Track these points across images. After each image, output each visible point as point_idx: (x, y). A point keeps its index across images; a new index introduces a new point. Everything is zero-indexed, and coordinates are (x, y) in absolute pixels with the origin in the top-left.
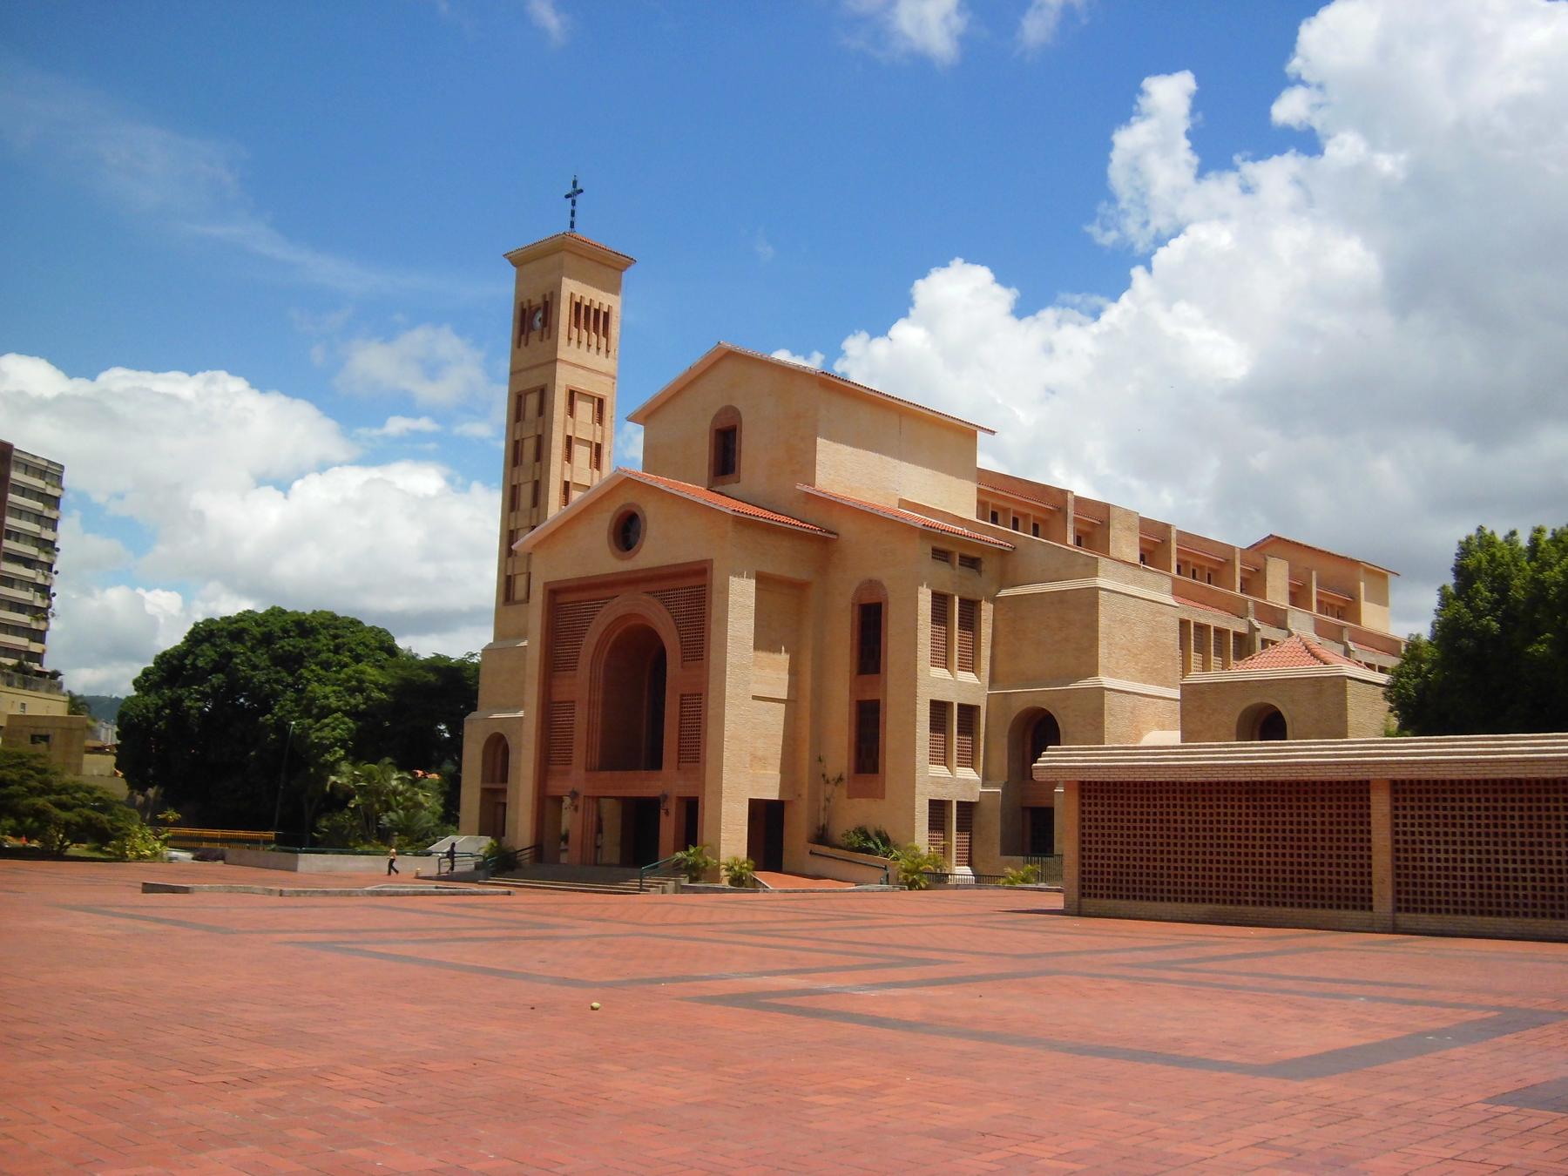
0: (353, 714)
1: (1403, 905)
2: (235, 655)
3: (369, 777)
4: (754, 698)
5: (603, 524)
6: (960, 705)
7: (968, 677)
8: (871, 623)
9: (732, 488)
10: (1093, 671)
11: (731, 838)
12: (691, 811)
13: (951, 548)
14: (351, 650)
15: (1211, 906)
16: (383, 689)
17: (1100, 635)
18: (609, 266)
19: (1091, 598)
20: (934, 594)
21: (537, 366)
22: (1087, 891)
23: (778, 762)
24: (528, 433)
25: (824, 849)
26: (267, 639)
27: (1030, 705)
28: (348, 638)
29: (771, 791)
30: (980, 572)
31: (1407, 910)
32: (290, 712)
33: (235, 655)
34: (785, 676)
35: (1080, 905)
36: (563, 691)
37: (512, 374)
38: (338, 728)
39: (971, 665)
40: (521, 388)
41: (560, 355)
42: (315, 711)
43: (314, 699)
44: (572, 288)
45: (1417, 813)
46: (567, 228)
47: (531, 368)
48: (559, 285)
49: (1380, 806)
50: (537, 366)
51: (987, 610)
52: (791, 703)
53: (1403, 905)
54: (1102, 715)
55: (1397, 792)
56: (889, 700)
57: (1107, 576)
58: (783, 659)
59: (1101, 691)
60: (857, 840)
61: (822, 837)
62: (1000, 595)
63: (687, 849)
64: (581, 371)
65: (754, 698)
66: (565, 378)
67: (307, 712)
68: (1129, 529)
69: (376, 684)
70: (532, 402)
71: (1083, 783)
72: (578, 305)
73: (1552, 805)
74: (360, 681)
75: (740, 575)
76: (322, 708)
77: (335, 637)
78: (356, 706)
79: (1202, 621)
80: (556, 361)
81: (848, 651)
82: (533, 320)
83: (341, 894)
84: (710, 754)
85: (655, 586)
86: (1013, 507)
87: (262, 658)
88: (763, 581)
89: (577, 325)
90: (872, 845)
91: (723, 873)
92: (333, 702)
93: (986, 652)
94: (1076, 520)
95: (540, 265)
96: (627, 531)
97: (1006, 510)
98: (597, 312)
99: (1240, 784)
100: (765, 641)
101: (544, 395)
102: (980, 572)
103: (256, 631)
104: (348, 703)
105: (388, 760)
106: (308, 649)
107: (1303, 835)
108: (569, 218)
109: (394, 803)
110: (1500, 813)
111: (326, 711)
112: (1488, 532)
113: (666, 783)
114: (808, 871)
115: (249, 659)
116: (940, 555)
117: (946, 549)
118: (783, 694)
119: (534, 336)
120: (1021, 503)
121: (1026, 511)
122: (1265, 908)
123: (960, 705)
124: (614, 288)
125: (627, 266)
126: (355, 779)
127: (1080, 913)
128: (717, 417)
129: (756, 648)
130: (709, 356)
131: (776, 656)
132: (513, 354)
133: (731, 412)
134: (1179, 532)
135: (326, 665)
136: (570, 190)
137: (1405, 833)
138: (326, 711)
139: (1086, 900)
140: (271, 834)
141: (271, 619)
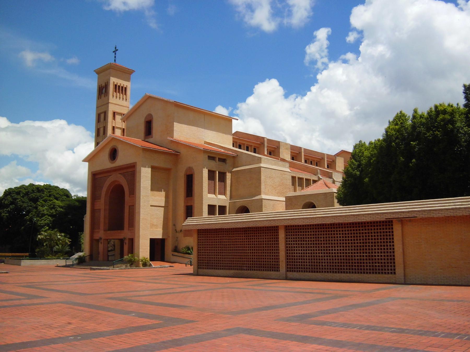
0: (52, 216)
1: (289, 269)
2: (18, 199)
3: (50, 235)
4: (151, 206)
5: (106, 155)
6: (219, 206)
7: (222, 197)
8: (190, 180)
9: (151, 140)
10: (260, 194)
11: (144, 251)
12: (132, 241)
13: (215, 156)
14: (54, 196)
15: (236, 271)
16: (62, 207)
17: (262, 182)
18: (126, 73)
19: (258, 171)
20: (209, 171)
21: (104, 105)
22: (200, 267)
23: (162, 226)
24: (101, 126)
25: (176, 254)
26: (27, 194)
27: (244, 205)
28: (54, 192)
29: (158, 235)
30: (226, 163)
31: (290, 271)
32: (34, 215)
33: (18, 199)
34: (164, 199)
35: (198, 271)
36: (97, 207)
37: (97, 108)
38: (47, 220)
39: (224, 194)
40: (99, 112)
41: (110, 101)
42: (40, 215)
43: (40, 211)
44: (113, 80)
45: (267, 237)
46: (113, 62)
47: (102, 106)
48: (109, 79)
49: (282, 235)
50: (104, 105)
51: (229, 176)
52: (166, 207)
53: (289, 269)
54: (262, 207)
55: (287, 230)
56: (195, 205)
57: (265, 163)
58: (163, 193)
59: (262, 199)
60: (185, 250)
61: (176, 250)
62: (233, 170)
63: (128, 255)
64: (117, 106)
65: (151, 206)
66: (112, 108)
67: (38, 216)
68: (287, 149)
69: (59, 206)
70: (102, 116)
71: (199, 230)
72: (116, 85)
73: (333, 233)
74: (54, 205)
75: (145, 167)
76: (42, 214)
77: (50, 192)
78: (53, 213)
79: (301, 176)
80: (108, 103)
81: (183, 190)
82: (103, 91)
83: (5, 273)
84: (136, 224)
85: (122, 172)
86: (246, 143)
87: (26, 199)
88: (154, 168)
89: (116, 92)
90: (189, 252)
91: (140, 262)
92: (45, 212)
93: (228, 188)
94: (268, 146)
95: (104, 72)
96: (113, 154)
97: (244, 144)
98: (122, 87)
99: (240, 228)
100: (155, 187)
101: (105, 113)
102: (226, 163)
103: (24, 191)
104: (50, 212)
105: (56, 230)
106: (40, 196)
107: (342, 242)
108: (114, 59)
109: (58, 243)
110: (317, 236)
111: (43, 215)
112: (363, 142)
113: (125, 234)
114: (172, 261)
115: (21, 200)
116: (211, 158)
117: (217, 157)
118: (163, 204)
119: (103, 95)
120: (247, 141)
121: (244, 142)
122: (249, 271)
123: (219, 206)
124: (128, 80)
125: (132, 73)
126: (46, 236)
127: (198, 275)
128: (146, 118)
129: (152, 189)
130: (143, 98)
131: (160, 193)
132: (97, 101)
133: (150, 115)
134: (304, 149)
135: (45, 201)
136: (114, 50)
137: (289, 244)
138: (43, 215)
139: (199, 270)
140: (28, 254)
141: (29, 187)
